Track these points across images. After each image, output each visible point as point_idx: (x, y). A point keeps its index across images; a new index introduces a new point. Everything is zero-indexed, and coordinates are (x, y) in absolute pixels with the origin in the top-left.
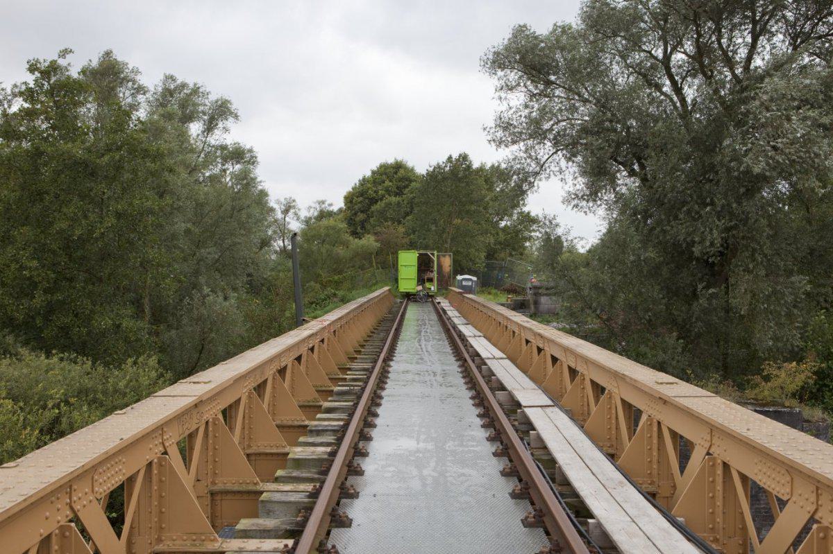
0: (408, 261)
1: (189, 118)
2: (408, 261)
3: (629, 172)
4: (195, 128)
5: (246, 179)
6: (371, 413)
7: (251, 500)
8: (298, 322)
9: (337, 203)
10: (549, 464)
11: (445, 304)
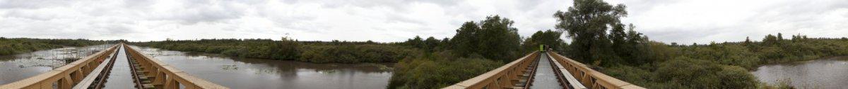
0: (542, 46)
1: (507, 24)
2: (542, 46)
3: (639, 37)
4: (508, 25)
5: (516, 33)
6: (536, 69)
7: (517, 82)
8: (525, 56)
9: (530, 37)
10: (564, 77)
11: (548, 53)
